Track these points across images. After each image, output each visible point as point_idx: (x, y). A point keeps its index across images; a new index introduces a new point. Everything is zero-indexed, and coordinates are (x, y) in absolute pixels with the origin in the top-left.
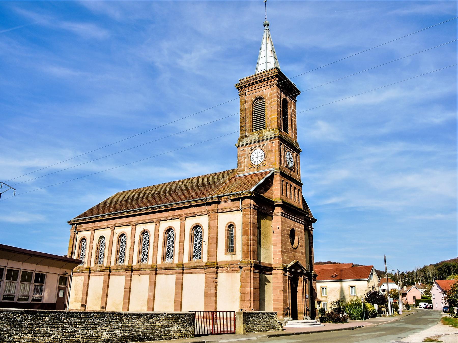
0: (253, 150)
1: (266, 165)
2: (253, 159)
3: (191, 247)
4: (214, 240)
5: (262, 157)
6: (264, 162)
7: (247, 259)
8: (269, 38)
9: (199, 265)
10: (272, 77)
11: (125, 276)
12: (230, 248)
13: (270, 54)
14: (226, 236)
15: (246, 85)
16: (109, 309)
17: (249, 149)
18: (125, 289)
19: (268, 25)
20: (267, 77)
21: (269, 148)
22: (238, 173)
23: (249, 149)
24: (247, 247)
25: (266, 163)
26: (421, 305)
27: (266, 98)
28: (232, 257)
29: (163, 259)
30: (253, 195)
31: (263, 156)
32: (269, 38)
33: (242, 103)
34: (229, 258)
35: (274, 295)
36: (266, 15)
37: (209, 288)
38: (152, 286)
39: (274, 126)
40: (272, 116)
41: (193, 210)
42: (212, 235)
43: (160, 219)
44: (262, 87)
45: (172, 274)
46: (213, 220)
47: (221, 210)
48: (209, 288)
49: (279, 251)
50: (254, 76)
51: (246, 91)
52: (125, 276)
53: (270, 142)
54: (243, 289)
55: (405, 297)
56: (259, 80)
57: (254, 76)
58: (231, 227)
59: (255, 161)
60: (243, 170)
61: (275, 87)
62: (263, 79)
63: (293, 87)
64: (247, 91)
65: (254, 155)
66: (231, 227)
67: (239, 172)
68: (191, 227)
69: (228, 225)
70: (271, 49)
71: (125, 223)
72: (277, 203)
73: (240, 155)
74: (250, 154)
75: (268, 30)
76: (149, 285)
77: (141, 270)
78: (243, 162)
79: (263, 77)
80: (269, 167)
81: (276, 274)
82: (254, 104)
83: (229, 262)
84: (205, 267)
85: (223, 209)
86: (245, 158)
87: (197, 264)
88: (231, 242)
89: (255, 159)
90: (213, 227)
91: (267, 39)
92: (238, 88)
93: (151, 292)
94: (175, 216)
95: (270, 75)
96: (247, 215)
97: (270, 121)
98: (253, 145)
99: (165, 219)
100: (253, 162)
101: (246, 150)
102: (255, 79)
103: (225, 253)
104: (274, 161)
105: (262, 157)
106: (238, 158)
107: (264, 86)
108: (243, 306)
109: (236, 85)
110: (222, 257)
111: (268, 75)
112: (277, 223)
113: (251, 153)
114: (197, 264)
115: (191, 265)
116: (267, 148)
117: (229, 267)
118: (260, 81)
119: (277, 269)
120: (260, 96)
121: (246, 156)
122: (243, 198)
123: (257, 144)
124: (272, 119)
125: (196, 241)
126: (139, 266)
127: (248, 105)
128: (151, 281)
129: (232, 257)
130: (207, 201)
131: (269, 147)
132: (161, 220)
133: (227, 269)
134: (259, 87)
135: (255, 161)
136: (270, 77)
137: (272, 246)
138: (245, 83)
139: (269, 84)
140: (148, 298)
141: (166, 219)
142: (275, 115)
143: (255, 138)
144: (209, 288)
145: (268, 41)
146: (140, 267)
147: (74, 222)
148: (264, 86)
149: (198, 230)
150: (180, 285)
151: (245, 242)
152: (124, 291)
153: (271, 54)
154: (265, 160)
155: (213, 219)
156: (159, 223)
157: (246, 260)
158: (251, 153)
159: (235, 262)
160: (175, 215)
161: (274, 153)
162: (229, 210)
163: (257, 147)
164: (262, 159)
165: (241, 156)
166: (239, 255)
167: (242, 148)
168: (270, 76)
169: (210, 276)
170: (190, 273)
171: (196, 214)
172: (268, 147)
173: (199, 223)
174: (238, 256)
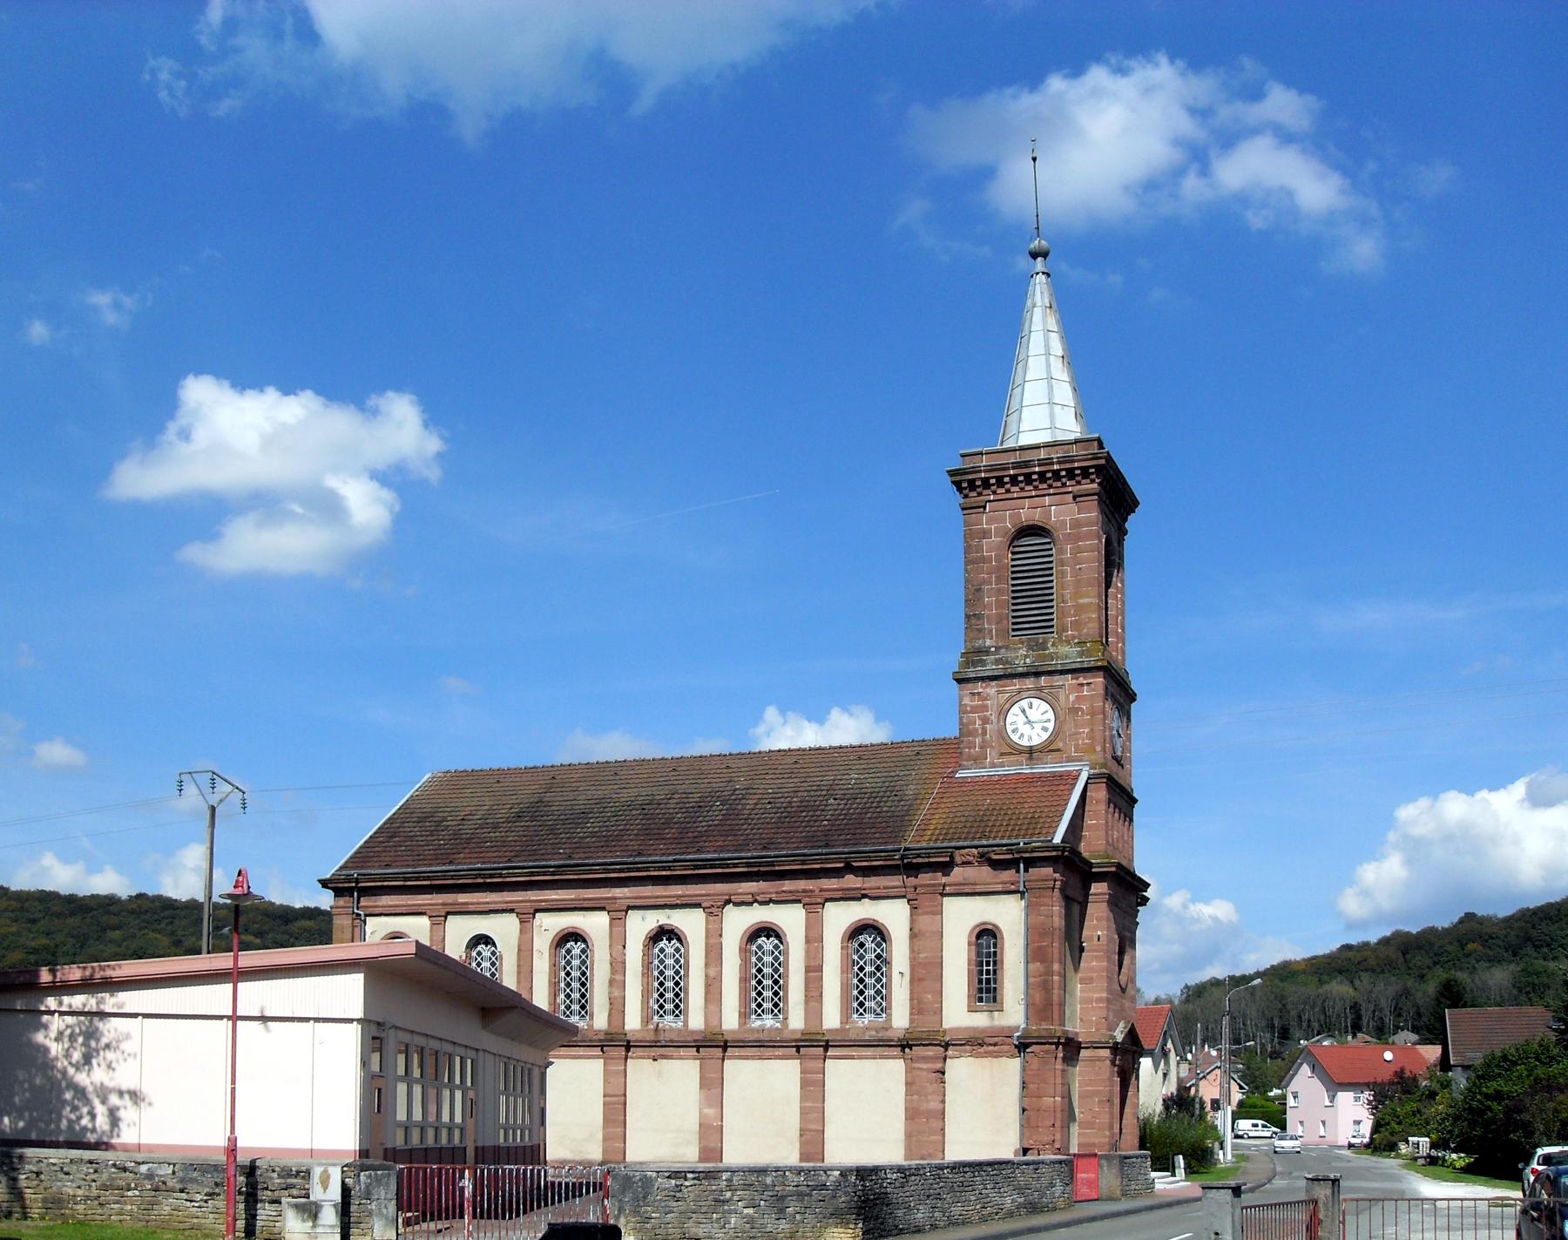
0: (1016, 699)
1: (1058, 750)
2: (1015, 726)
3: (845, 988)
4: (927, 973)
5: (1046, 725)
6: (1050, 741)
7: (1043, 1023)
8: (1051, 307)
9: (880, 1035)
10: (1085, 472)
11: (602, 1060)
12: (986, 989)
13: (1061, 373)
14: (969, 960)
15: (988, 479)
16: (737, 1153)
17: (999, 692)
18: (604, 1096)
19: (1045, 255)
20: (1068, 466)
21: (1071, 700)
22: (960, 765)
23: (999, 692)
24: (1043, 992)
25: (1060, 745)
26: (1240, 1127)
27: (1059, 535)
28: (992, 1018)
29: (744, 1016)
30: (1066, 853)
31: (1049, 720)
32: (1051, 307)
33: (972, 537)
34: (980, 1020)
35: (1082, 1113)
36: (1037, 216)
37: (923, 1098)
38: (713, 1090)
39: (1085, 631)
40: (1081, 597)
41: (851, 881)
42: (926, 957)
43: (727, 897)
44: (1044, 495)
45: (782, 1059)
46: (927, 913)
47: (955, 887)
48: (923, 1098)
49: (1099, 1000)
50: (1016, 450)
51: (987, 498)
52: (602, 1060)
53: (1074, 681)
54: (1034, 1099)
55: (60, 1043)
56: (1037, 469)
57: (1016, 450)
58: (986, 936)
59: (1022, 735)
60: (978, 756)
61: (1093, 502)
62: (1054, 472)
63: (1127, 493)
64: (992, 497)
65: (1014, 717)
66: (986, 936)
67: (965, 763)
68: (844, 929)
69: (977, 930)
70: (1060, 353)
71: (578, 900)
72: (1100, 867)
73: (968, 708)
74: (1003, 713)
75: (1048, 275)
76: (701, 1088)
77: (659, 1045)
78: (980, 731)
79: (1053, 464)
80: (1070, 759)
81: (1091, 1060)
82: (1014, 547)
83: (984, 1030)
84: (905, 1045)
85: (961, 884)
86: (985, 721)
87: (874, 1033)
88: (984, 976)
89: (1025, 729)
90: (928, 934)
91: (1048, 310)
92: (958, 484)
93: (710, 1106)
94: (784, 892)
95: (1078, 461)
96: (1042, 908)
97: (1072, 612)
98: (1017, 685)
99: (749, 898)
100: (1015, 738)
101: (988, 695)
102: (1026, 464)
103: (969, 1006)
104: (1086, 741)
105: (1046, 725)
106: (961, 718)
107: (1052, 491)
108: (1031, 1141)
109: (952, 473)
110: (957, 1012)
111: (1073, 461)
112: (1095, 922)
113: (1007, 706)
114: (874, 1033)
115: (852, 1036)
116: (1062, 697)
117: (977, 1043)
118: (1042, 475)
119: (1095, 1046)
120: (1036, 523)
121: (992, 714)
122: (1030, 863)
123: (1029, 683)
124: (1080, 609)
125: (861, 969)
126: (652, 1033)
127: (993, 546)
128: (707, 1075)
129: (992, 1018)
130: (909, 860)
131: (1072, 698)
132: (728, 902)
133: (974, 1048)
134: (1033, 493)
135: (1022, 735)
136: (1077, 468)
137: (1079, 986)
138: (985, 471)
139: (1070, 489)
140: (700, 1125)
141: (751, 900)
142: (1091, 594)
143: (1023, 661)
144: (921, 1096)
145: (1049, 320)
146: (656, 1035)
147: (354, 885)
148: (1052, 491)
149: (868, 939)
150: (813, 1089)
151: (1038, 979)
152: (604, 1105)
153: (1064, 370)
154: (1056, 734)
155: (928, 910)
156: (723, 909)
157: (1042, 1027)
158: (1007, 706)
159: (1006, 1033)
160: (784, 889)
161: (1088, 717)
162: (979, 888)
163: (1028, 690)
164: (1045, 729)
165: (971, 712)
166: (1016, 1012)
167: (979, 687)
168: (1076, 465)
169: (925, 1066)
170: (852, 1058)
171: (863, 892)
172: (1068, 697)
173: (875, 918)
174: (1013, 1013)
